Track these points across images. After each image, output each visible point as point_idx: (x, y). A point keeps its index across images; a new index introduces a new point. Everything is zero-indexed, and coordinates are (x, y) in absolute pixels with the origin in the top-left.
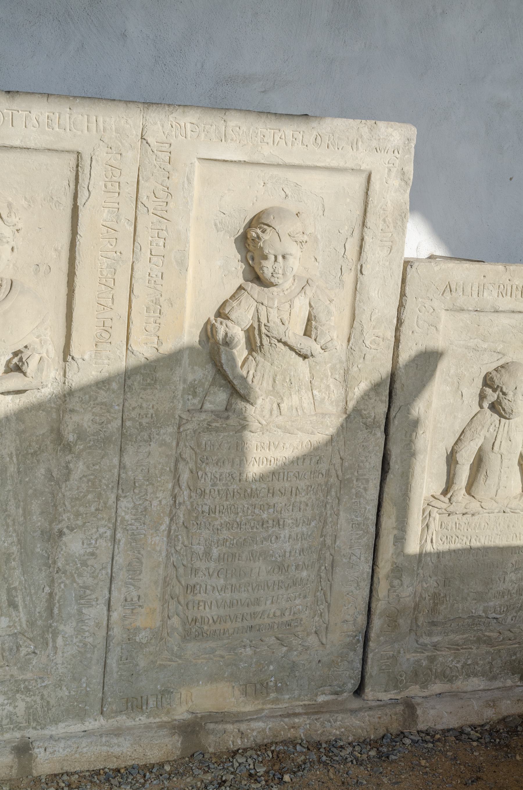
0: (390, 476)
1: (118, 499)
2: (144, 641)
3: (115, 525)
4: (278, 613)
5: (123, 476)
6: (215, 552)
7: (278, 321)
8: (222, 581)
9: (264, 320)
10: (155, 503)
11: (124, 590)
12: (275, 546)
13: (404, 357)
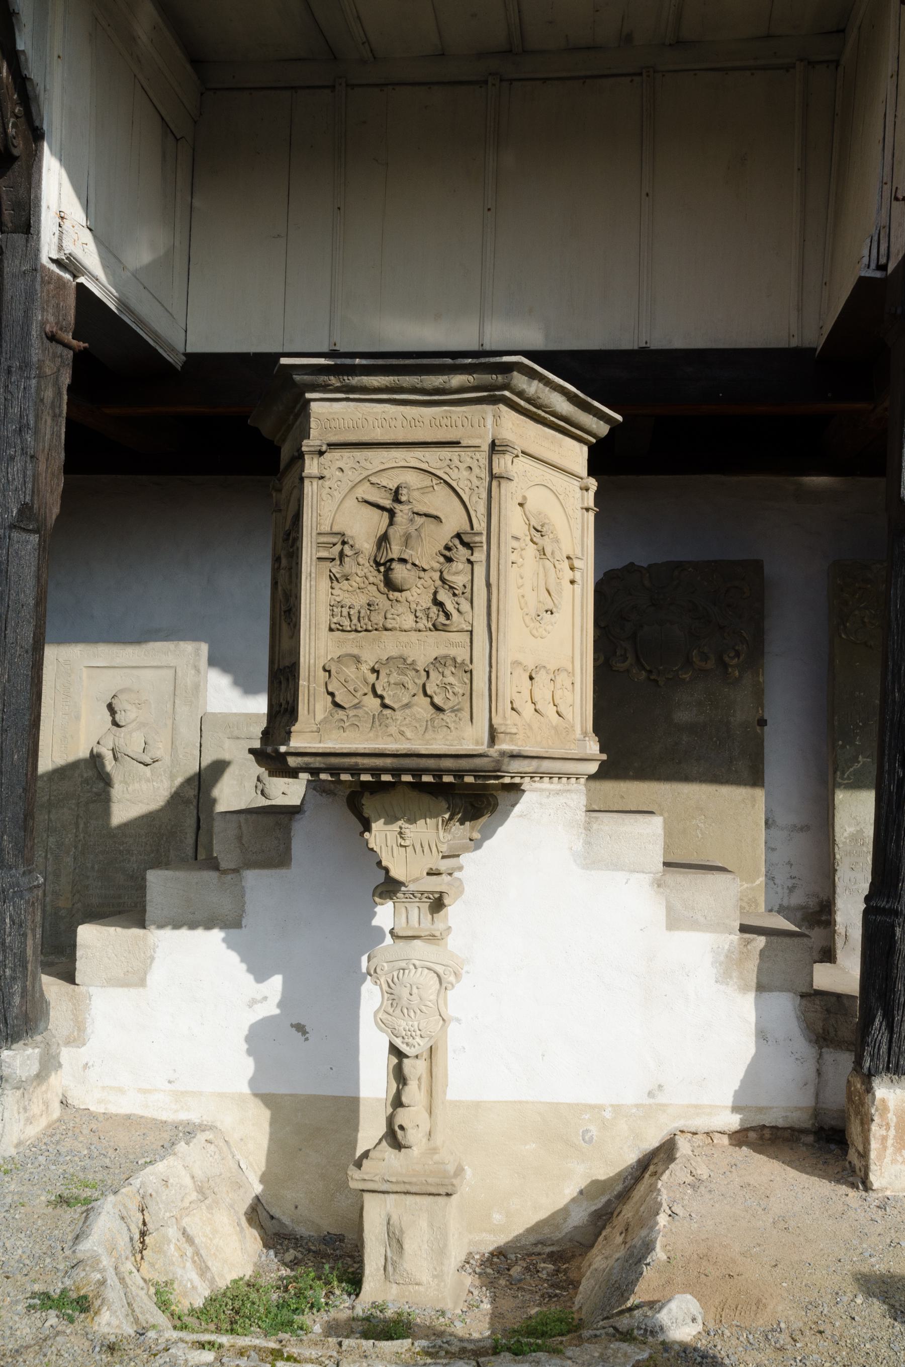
0: (201, 831)
1: (48, 836)
2: (64, 915)
3: (46, 850)
4: (133, 905)
5: (50, 825)
6: (96, 867)
7: (124, 745)
8: (100, 883)
9: (117, 744)
10: (67, 840)
11: (52, 886)
13: (204, 764)
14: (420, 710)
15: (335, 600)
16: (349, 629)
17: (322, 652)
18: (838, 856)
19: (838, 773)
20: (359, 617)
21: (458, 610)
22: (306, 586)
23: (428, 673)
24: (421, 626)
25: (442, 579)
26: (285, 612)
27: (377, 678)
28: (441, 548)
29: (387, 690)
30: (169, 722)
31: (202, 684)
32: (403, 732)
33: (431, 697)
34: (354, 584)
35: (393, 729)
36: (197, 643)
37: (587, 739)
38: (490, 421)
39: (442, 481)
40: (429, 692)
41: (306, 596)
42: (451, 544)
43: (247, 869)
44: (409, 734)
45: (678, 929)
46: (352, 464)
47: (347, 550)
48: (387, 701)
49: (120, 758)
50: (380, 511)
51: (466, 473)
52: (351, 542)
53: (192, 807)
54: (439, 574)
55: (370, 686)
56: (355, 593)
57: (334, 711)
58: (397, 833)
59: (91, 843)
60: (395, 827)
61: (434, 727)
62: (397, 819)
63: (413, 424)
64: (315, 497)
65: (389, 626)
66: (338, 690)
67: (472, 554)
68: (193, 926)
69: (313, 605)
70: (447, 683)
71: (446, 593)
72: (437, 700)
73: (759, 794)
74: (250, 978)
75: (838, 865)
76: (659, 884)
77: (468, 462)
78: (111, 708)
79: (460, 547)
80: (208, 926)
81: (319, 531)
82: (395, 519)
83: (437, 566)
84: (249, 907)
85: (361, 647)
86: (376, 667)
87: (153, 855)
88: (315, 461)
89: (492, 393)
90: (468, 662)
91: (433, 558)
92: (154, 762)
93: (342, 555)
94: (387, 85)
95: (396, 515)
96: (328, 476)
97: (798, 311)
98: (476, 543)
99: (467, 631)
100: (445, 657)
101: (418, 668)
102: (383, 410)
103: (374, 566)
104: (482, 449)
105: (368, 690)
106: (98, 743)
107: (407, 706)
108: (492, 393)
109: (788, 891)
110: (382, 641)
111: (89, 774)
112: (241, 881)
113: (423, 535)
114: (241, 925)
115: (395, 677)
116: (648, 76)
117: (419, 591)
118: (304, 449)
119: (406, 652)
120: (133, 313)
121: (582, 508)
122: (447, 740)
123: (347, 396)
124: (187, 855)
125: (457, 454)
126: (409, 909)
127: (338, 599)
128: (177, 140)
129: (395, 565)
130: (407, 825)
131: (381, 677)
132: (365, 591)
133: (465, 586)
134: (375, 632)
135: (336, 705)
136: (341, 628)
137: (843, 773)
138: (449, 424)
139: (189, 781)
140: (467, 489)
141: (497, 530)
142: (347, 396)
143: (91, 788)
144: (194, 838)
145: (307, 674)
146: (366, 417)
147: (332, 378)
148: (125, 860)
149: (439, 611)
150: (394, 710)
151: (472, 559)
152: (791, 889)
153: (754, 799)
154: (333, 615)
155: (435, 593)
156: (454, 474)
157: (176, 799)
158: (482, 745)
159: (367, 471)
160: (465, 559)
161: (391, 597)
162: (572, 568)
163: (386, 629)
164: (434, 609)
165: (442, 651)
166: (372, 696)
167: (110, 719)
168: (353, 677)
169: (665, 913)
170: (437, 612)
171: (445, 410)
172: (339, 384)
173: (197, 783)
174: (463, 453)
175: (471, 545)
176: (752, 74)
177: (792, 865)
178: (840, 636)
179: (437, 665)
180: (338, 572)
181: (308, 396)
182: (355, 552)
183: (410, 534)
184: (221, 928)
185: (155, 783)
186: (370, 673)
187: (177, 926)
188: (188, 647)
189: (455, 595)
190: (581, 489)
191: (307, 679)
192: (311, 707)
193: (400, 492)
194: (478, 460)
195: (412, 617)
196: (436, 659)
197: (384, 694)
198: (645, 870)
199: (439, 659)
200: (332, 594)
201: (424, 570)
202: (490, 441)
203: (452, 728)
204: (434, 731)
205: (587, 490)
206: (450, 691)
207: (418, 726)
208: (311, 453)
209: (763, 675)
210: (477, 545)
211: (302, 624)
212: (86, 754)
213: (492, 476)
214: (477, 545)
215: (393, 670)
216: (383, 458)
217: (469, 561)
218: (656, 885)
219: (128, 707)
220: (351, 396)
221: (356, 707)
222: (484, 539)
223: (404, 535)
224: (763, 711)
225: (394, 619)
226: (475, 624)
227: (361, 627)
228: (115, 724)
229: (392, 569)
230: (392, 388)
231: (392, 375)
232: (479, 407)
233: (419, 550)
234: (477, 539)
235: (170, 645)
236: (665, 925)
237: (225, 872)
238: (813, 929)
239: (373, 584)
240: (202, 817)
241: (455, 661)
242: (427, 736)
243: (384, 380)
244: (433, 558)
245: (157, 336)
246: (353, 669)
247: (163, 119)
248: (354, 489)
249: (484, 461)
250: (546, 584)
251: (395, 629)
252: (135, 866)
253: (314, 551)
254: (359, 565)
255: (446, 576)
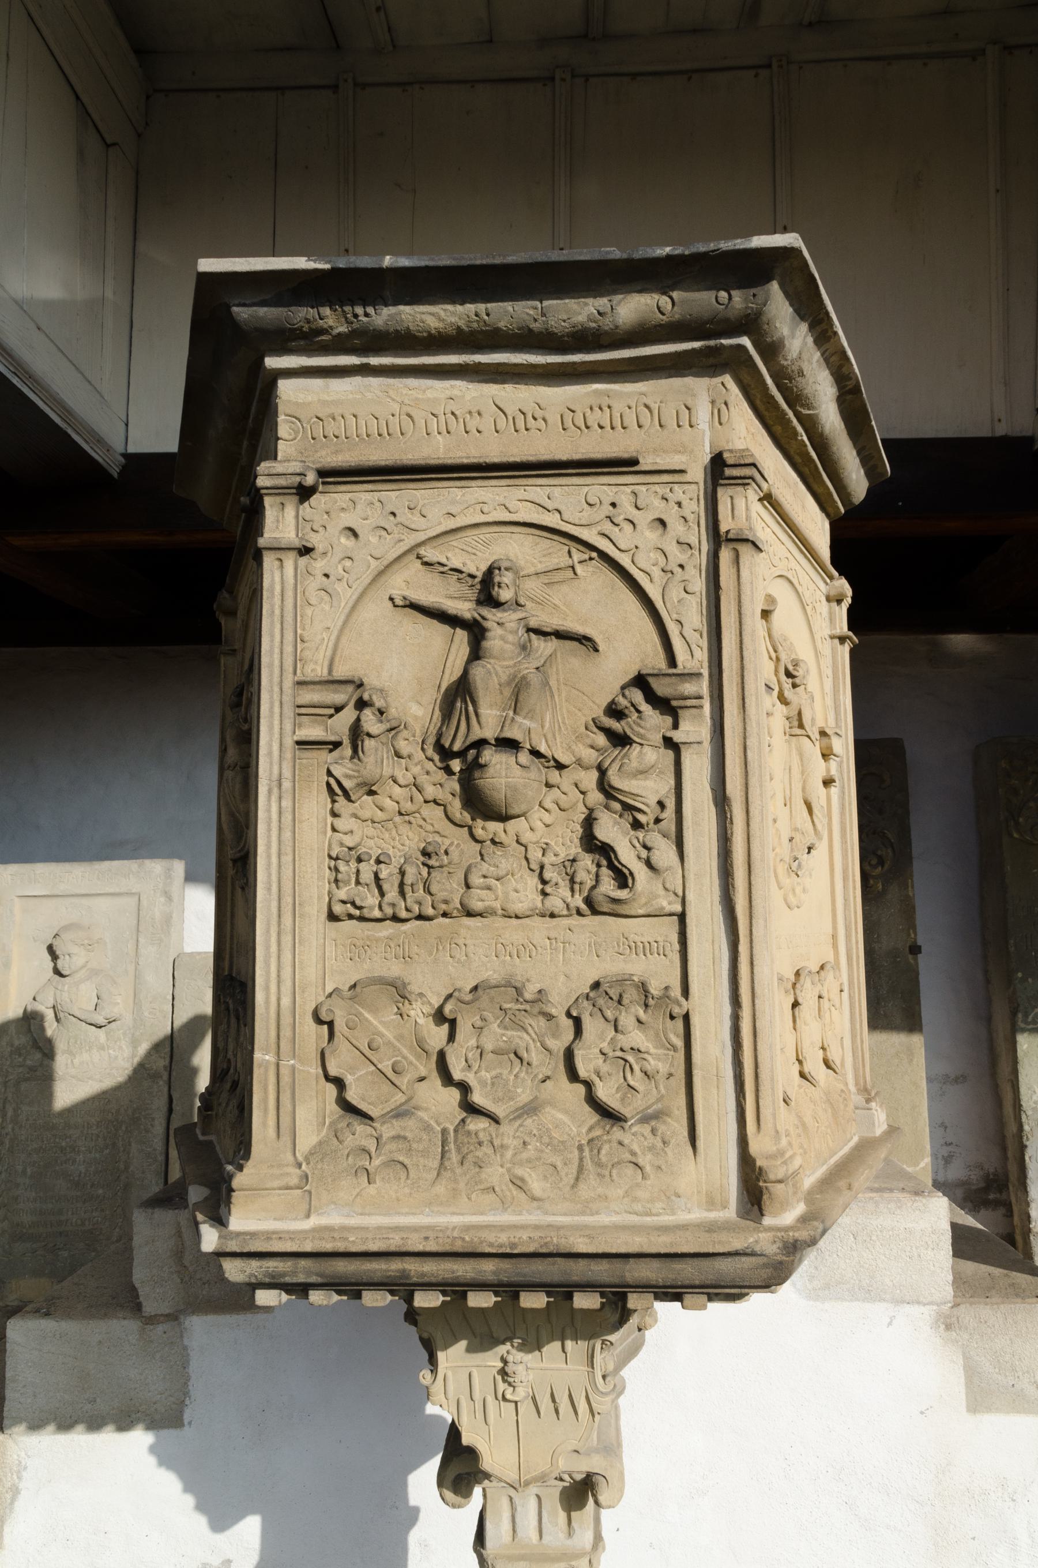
0: (173, 1115)
4: (79, 1222)
7: (68, 1000)
8: (34, 1194)
9: (59, 1001)
12: (72, 1167)
13: (178, 1023)
14: (560, 1116)
15: (342, 845)
16: (377, 913)
17: (311, 973)
18: (1026, 1128)
19: (1020, 1015)
20: (402, 885)
21: (649, 864)
22: (269, 811)
23: (577, 1022)
24: (555, 903)
25: (605, 787)
26: (235, 861)
27: (451, 1037)
28: (599, 712)
29: (475, 1068)
30: (131, 968)
31: (174, 915)
32: (522, 1180)
33: (588, 1085)
34: (388, 803)
35: (495, 1174)
36: (168, 861)
37: (873, 1104)
38: (703, 413)
39: (594, 555)
40: (583, 1072)
41: (269, 837)
42: (623, 702)
43: (193, 1313)
44: (536, 1186)
45: (989, 1410)
46: (377, 517)
47: (370, 721)
48: (477, 1098)
49: (63, 1019)
50: (446, 629)
51: (650, 536)
52: (379, 703)
53: (162, 1083)
54: (595, 775)
55: (434, 1058)
56: (390, 825)
57: (344, 1124)
58: (495, 1371)
59: (23, 1137)
60: (491, 1359)
61: (599, 1164)
62: (498, 1342)
63: (521, 424)
64: (289, 594)
65: (477, 905)
66: (352, 1070)
67: (676, 726)
68: (95, 1424)
69: (287, 859)
70: (626, 1047)
71: (616, 823)
72: (604, 1093)
73: (917, 1041)
74: (201, 1522)
75: (1028, 1139)
76: (948, 1324)
77: (657, 508)
78: (51, 950)
79: (645, 707)
80: (124, 1425)
81: (299, 677)
82: (485, 644)
83: (591, 756)
84: (197, 1386)
85: (407, 958)
86: (448, 1009)
87: (107, 1151)
88: (290, 511)
89: (712, 343)
90: (676, 992)
91: (579, 738)
92: (109, 1023)
93: (356, 732)
94: (411, 84)
95: (488, 634)
96: (320, 547)
97: (1006, 386)
98: (686, 698)
99: (671, 915)
100: (622, 981)
101: (553, 1011)
102: (448, 393)
103: (436, 758)
104: (687, 477)
105: (428, 1067)
106: (34, 999)
107: (531, 1109)
108: (712, 343)
109: (943, 1162)
110: (461, 942)
111: (21, 1040)
112: (182, 1336)
113: (553, 683)
114: (182, 1420)
115: (495, 1035)
116: (781, 66)
117: (547, 818)
118: (261, 482)
119: (522, 969)
120: (10, 356)
121: (832, 637)
122: (635, 1199)
123: (365, 360)
124: (155, 1150)
125: (628, 490)
126: (517, 1500)
127: (349, 841)
128: (108, 146)
129: (488, 755)
130: (519, 1356)
131: (460, 1036)
132: (416, 820)
133: (661, 805)
134: (441, 920)
135: (349, 1108)
136: (357, 912)
137: (1026, 1015)
138: (607, 423)
139: (157, 1047)
140: (656, 572)
141: (736, 665)
142: (365, 360)
143: (25, 1060)
144: (164, 1125)
145: (273, 1033)
146: (410, 410)
147: (326, 311)
148: (69, 1160)
149: (599, 866)
150: (496, 1120)
151: (677, 736)
152: (948, 1160)
153: (910, 1053)
154: (336, 881)
155: (589, 822)
156: (625, 537)
157: (141, 1072)
158: (724, 1206)
159: (415, 535)
160: (658, 739)
161: (479, 832)
162: (825, 756)
163: (470, 914)
164: (587, 862)
165: (608, 967)
166: (438, 1082)
167: (52, 965)
168: (389, 1035)
169: (963, 1380)
170: (594, 869)
171: (596, 391)
172: (343, 329)
173: (168, 1049)
174: (643, 488)
175: (674, 703)
176: (925, 64)
177: (946, 1127)
178: (1011, 835)
179: (601, 1002)
180: (348, 776)
181: (272, 362)
182: (388, 726)
183: (524, 678)
184: (149, 1428)
185: (111, 1051)
186: (432, 1025)
187: (65, 1426)
188: (156, 866)
189: (637, 825)
190: (829, 599)
191: (274, 1046)
192: (285, 1120)
193: (497, 579)
194: (679, 504)
195: (533, 882)
196: (596, 985)
197: (471, 1079)
198: (921, 1299)
199: (605, 987)
200: (334, 830)
201: (560, 766)
202: (707, 459)
203: (648, 1168)
204: (601, 1176)
205: (839, 602)
206: (636, 1068)
207: (559, 1164)
208: (279, 491)
209: (913, 887)
210: (689, 703)
211: (259, 905)
212: (20, 1013)
213: (717, 538)
214: (689, 703)
215: (488, 1015)
216: (453, 502)
217: (669, 743)
218: (943, 1327)
219: (74, 949)
220: (375, 361)
221: (399, 1113)
222: (704, 687)
223: (509, 683)
224: (916, 935)
225: (489, 888)
226: (690, 897)
227: (407, 910)
228: (57, 972)
229: (482, 766)
230: (473, 333)
231: (473, 301)
232: (676, 383)
233: (548, 717)
234: (688, 688)
235: (133, 865)
236: (964, 1403)
237: (151, 1320)
238: (979, 1212)
239: (435, 802)
240: (175, 1096)
241: (646, 992)
242: (585, 1190)
243: (453, 313)
244: (579, 738)
245: (67, 411)
246: (390, 1015)
247: (78, 98)
248: (383, 579)
249: (694, 506)
250: (804, 790)
251: (493, 912)
252: (82, 1168)
253: (288, 727)
254: (398, 755)
255: (614, 778)
